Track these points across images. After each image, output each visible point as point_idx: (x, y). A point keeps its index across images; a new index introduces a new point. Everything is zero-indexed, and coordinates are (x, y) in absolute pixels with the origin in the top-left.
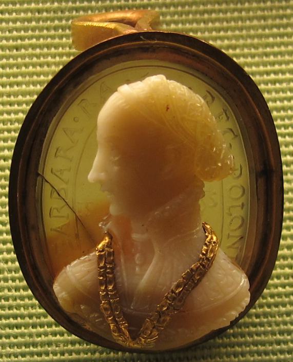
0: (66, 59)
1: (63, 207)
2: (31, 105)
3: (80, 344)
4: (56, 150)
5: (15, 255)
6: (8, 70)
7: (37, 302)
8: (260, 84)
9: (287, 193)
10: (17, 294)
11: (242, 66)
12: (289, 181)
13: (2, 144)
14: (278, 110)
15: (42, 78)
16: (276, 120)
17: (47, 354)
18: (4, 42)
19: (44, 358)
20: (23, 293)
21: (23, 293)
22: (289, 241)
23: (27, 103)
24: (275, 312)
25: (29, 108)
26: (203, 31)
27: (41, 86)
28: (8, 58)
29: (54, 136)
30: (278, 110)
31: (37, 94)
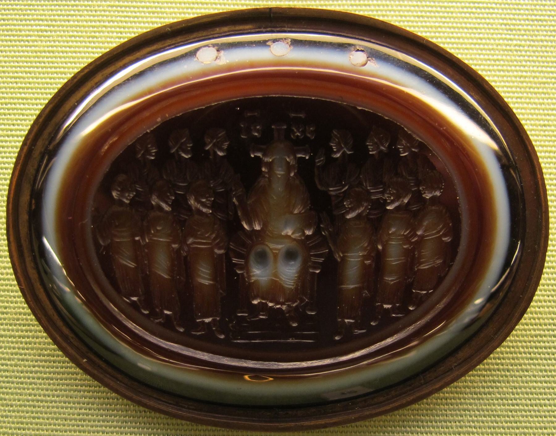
0: (481, 366)
5: (8, 254)
6: (5, 43)
7: (34, 317)
8: (522, 120)
14: (543, 158)
15: (85, 60)
16: (546, 175)
17: (43, 430)
18: (2, 22)
19: (41, 432)
20: (9, 276)
21: (9, 276)
24: (505, 414)
26: (437, 38)
27: (77, 69)
28: (5, 46)
29: (91, 112)
30: (543, 158)
31: (67, 79)
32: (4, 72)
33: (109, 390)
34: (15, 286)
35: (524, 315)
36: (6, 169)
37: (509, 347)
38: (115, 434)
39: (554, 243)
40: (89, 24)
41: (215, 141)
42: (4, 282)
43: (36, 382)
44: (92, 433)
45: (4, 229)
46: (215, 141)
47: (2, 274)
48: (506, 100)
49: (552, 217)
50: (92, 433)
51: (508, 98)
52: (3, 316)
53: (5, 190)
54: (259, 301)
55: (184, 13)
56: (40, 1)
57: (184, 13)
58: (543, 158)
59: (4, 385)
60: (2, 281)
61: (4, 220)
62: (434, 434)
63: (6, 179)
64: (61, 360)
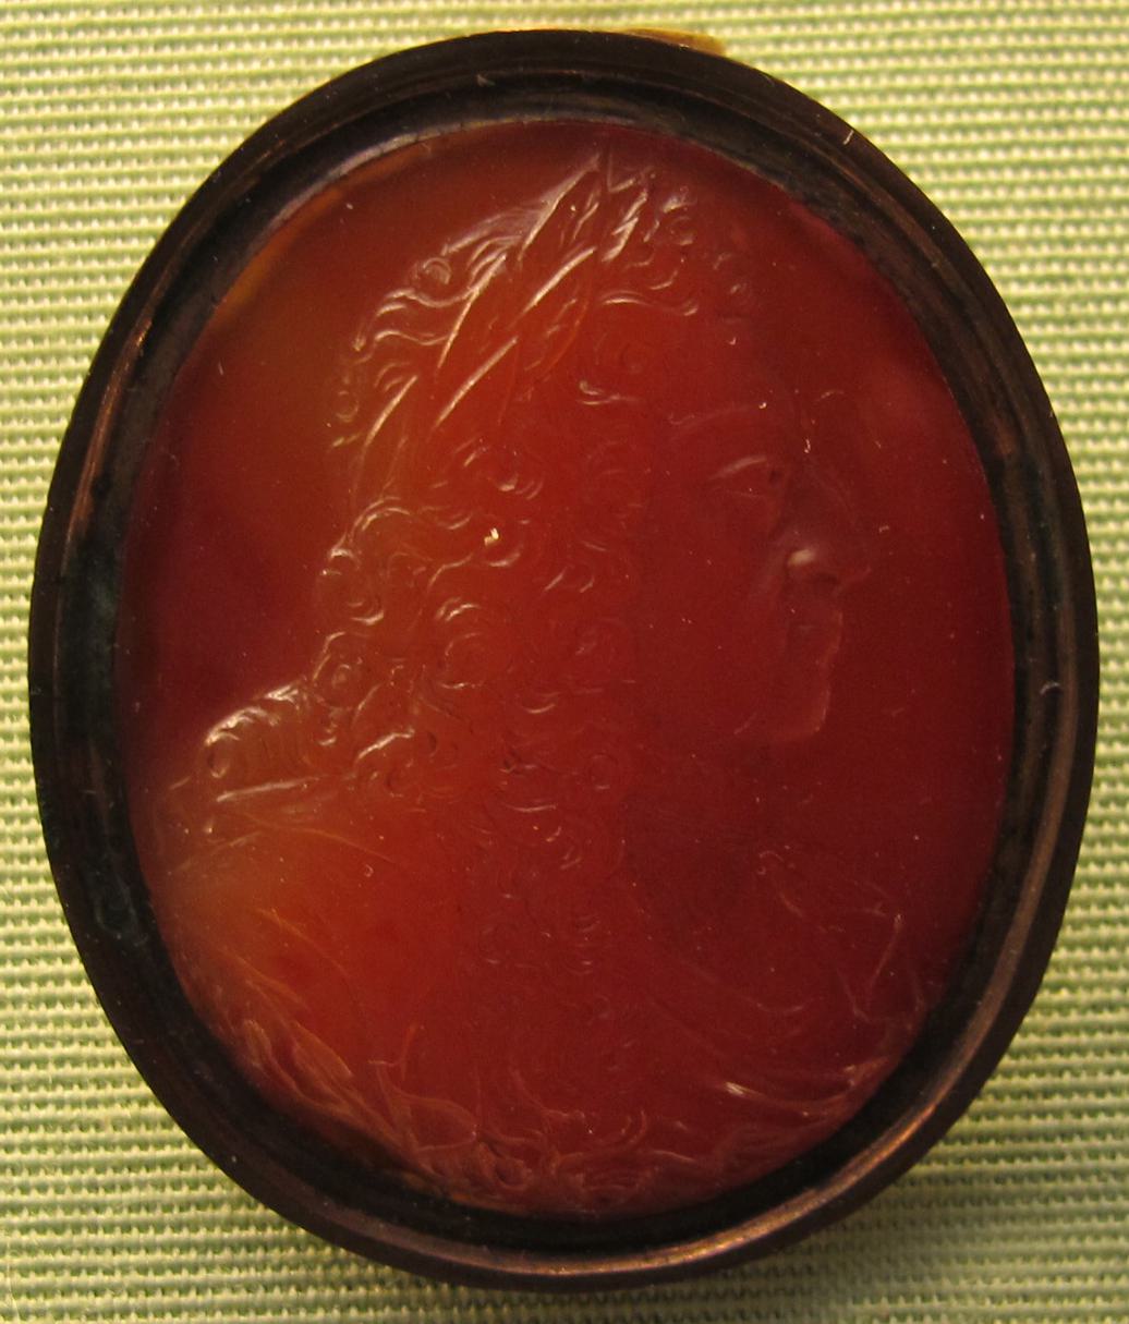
4: (33, 1319)
20: (68, 988)
21: (68, 988)
33: (353, 1255)
34: (66, 959)
35: (1068, 893)
36: (29, 475)
38: (133, 1316)
39: (1120, 647)
40: (169, 1276)
42: (67, 1012)
43: (11, 1183)
44: (151, 1317)
50: (151, 1317)
55: (381, 35)
57: (381, 35)
59: (15, 1304)
62: (928, 1320)
63: (28, 515)
64: (172, 1198)
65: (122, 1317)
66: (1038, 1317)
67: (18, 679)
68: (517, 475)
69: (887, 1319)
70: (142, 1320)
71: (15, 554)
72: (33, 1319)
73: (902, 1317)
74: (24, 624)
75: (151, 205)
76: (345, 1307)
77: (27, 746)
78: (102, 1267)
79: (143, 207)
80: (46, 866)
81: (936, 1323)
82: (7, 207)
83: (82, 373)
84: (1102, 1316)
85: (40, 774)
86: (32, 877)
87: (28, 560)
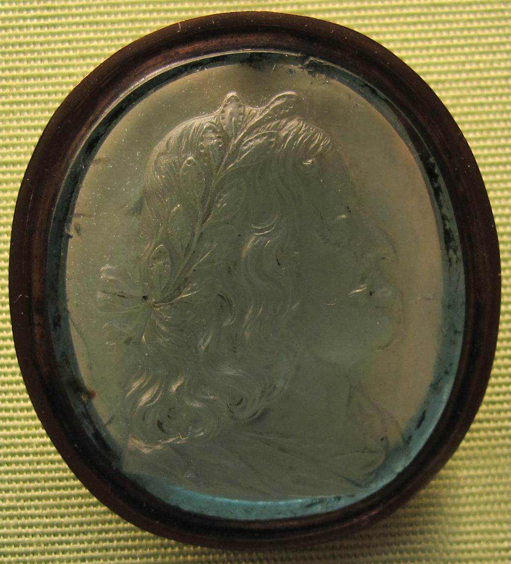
1: (110, 422)
2: (53, 113)
3: (135, 531)
4: (94, 561)
9: (504, 314)
10: (23, 512)
11: (419, 74)
12: (505, 243)
13: (1, 212)
22: (508, 335)
23: (49, 110)
25: (51, 115)
30: (500, 216)
31: (42, 128)
32: (7, 146)
37: (474, 439)
41: (152, 269)
45: (5, 295)
46: (152, 269)
47: (3, 500)
48: (407, 62)
49: (502, 234)
51: (409, 58)
52: (4, 424)
53: (7, 216)
54: (192, 404)
56: (24, 2)
58: (487, 174)
60: (3, 474)
61: (7, 255)
65: (67, 562)
66: (61, 560)
67: (6, 306)
68: (297, 95)
69: (33, 562)
70: (112, 562)
71: (7, 199)
72: (500, 562)
73: (399, 561)
74: (7, 264)
75: (67, 79)
76: (164, 556)
77: (9, 317)
78: (71, 524)
79: (64, 80)
80: (16, 361)
81: (420, 563)
82: (4, 116)
83: (38, 136)
84: (406, 560)
85: (14, 329)
86: (9, 366)
87: (5, 280)
